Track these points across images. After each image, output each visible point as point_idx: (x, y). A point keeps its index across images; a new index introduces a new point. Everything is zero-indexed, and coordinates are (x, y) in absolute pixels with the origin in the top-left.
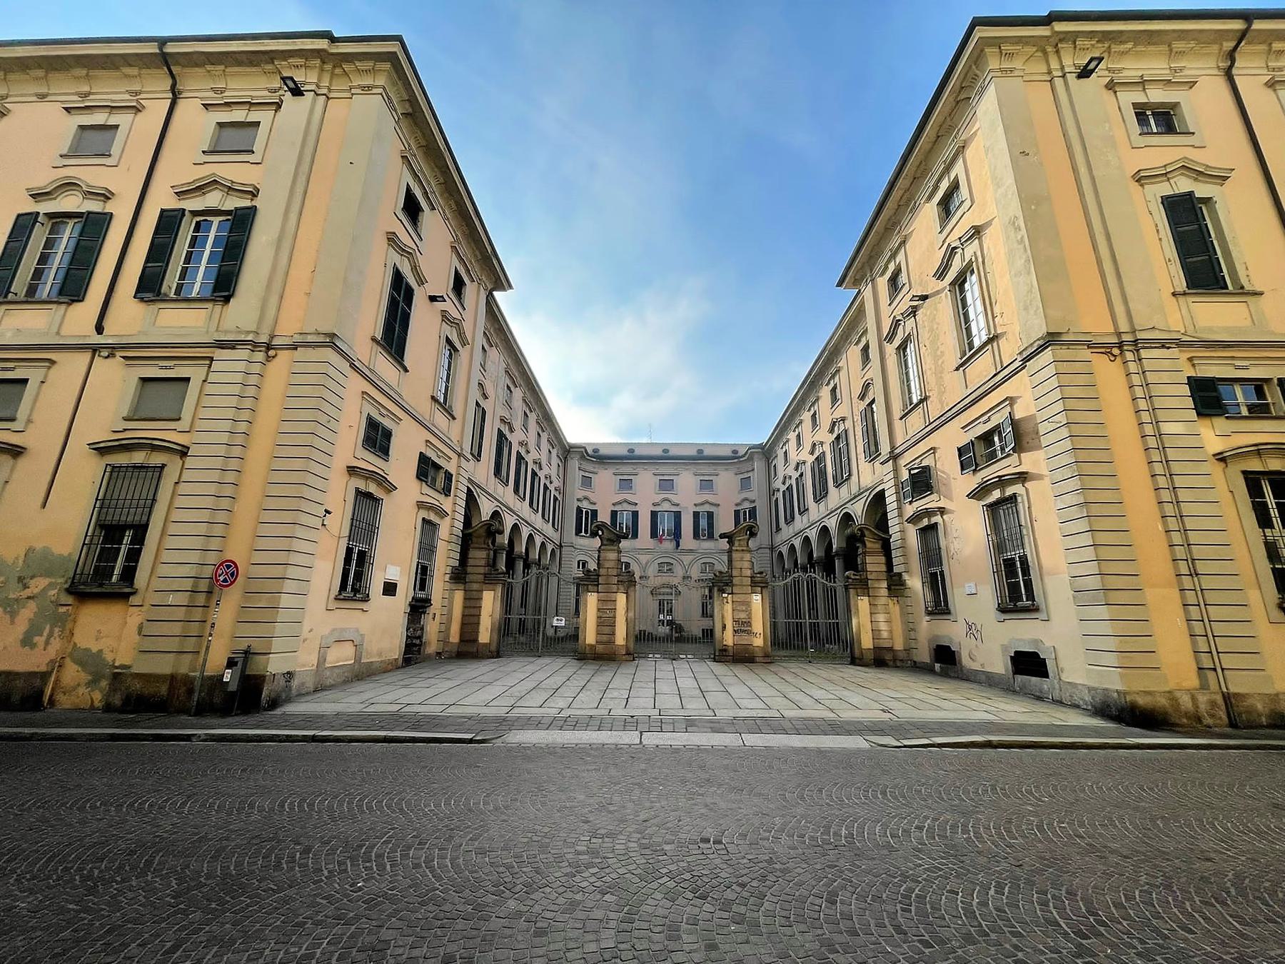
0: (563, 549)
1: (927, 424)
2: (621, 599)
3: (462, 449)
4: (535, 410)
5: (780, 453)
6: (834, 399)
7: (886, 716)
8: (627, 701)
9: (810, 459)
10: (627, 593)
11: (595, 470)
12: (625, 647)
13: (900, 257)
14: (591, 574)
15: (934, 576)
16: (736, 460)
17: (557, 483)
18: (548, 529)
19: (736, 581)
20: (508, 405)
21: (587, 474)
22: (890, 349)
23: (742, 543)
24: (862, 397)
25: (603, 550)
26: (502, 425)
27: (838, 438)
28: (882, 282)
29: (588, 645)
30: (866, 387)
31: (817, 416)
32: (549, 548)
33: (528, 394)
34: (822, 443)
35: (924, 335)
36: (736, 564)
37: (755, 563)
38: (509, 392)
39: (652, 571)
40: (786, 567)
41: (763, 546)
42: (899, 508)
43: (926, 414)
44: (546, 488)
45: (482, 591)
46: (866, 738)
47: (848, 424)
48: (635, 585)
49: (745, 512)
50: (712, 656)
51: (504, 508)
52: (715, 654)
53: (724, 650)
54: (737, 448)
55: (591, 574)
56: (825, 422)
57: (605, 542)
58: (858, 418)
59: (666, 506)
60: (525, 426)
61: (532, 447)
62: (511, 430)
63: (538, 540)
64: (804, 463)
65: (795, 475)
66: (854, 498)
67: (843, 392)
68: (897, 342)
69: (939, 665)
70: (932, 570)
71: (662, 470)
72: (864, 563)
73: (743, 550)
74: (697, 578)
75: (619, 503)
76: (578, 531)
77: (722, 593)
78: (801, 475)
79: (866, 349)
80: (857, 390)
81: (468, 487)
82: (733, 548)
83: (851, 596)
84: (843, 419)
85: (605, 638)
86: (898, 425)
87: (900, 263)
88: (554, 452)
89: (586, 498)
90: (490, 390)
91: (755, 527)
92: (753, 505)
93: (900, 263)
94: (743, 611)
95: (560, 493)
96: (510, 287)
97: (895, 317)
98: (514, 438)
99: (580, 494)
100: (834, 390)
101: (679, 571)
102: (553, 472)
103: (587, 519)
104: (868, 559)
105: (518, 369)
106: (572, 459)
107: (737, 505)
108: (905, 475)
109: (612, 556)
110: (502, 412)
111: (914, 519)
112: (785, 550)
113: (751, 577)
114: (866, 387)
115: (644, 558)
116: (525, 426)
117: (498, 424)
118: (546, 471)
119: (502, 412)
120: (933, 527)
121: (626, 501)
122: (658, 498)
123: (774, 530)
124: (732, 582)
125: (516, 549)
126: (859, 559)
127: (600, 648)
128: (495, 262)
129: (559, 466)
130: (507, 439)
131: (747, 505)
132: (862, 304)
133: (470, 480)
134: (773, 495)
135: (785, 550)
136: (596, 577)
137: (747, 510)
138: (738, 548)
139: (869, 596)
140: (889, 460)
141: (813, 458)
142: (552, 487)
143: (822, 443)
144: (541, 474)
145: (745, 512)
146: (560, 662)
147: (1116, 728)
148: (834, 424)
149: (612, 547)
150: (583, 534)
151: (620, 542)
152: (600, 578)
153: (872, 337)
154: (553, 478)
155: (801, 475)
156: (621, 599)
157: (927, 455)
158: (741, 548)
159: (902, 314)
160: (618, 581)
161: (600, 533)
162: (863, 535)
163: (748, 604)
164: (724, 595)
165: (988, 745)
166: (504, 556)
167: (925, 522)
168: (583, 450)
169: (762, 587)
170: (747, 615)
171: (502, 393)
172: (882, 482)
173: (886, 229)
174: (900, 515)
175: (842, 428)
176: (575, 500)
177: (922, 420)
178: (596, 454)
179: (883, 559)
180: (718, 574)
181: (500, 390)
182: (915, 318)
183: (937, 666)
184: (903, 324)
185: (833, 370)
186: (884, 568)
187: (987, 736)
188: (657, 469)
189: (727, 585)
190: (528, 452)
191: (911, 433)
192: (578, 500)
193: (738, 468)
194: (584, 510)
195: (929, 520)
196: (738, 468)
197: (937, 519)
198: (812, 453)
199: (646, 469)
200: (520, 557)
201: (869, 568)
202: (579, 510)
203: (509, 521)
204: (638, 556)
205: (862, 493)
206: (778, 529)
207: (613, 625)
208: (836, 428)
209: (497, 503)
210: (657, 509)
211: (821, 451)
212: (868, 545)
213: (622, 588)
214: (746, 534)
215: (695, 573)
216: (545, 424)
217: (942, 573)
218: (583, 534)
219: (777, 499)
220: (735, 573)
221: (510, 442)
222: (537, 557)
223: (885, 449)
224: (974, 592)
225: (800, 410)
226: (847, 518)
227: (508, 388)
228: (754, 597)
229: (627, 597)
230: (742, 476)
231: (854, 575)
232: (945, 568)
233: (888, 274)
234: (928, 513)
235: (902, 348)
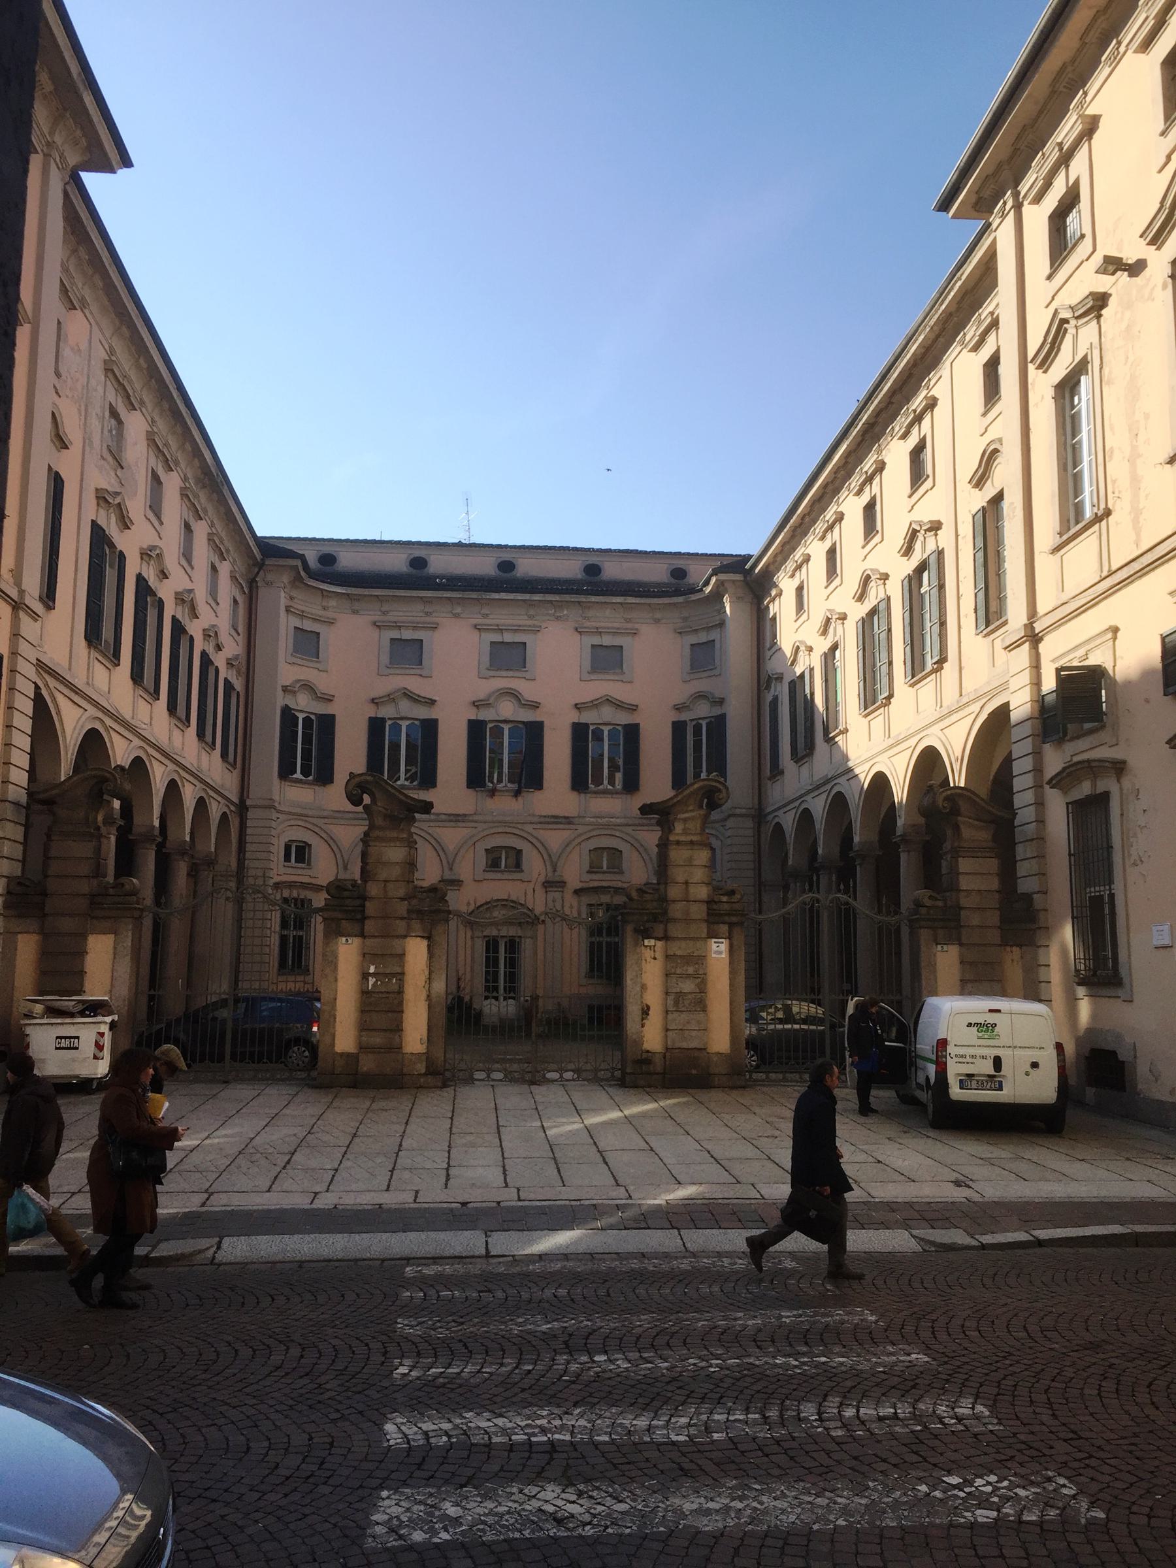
0: (250, 814)
1: (1105, 573)
2: (416, 951)
3: (22, 592)
4: (177, 463)
5: (786, 584)
6: (918, 473)
7: (960, 1194)
8: (448, 1175)
9: (858, 611)
10: (429, 938)
11: (330, 614)
12: (424, 1058)
13: (1078, 165)
14: (346, 894)
15: (1097, 902)
16: (681, 599)
17: (233, 647)
18: (213, 766)
19: (676, 910)
20: (116, 457)
21: (308, 625)
22: (1043, 385)
23: (690, 825)
24: (980, 480)
25: (378, 839)
26: (102, 512)
27: (922, 568)
28: (1037, 218)
29: (342, 1054)
30: (990, 458)
31: (878, 507)
32: (215, 810)
33: (162, 426)
34: (885, 577)
35: (1116, 367)
36: (679, 875)
37: (718, 852)
38: (113, 422)
39: (469, 867)
40: (790, 862)
41: (738, 811)
42: (1037, 754)
43: (1104, 551)
44: (206, 660)
45: (84, 937)
46: (915, 1232)
47: (945, 538)
48: (447, 921)
49: (697, 730)
50: (618, 1074)
51: (109, 722)
52: (623, 1070)
53: (645, 1060)
54: (680, 563)
55: (346, 894)
56: (894, 524)
57: (379, 821)
58: (966, 529)
59: (507, 710)
60: (155, 507)
61: (172, 560)
62: (125, 523)
63: (189, 795)
64: (843, 617)
65: (823, 645)
66: (950, 713)
67: (939, 459)
68: (1060, 368)
69: (1094, 1090)
70: (1093, 891)
71: (501, 617)
72: (955, 872)
73: (692, 842)
74: (579, 885)
75: (595, 705)
76: (286, 771)
77: (644, 938)
78: (835, 647)
79: (992, 367)
80: (969, 464)
81: (37, 687)
82: (672, 838)
83: (923, 942)
84: (935, 527)
85: (377, 1040)
86: (1045, 564)
87: (1077, 182)
88: (225, 569)
89: (308, 687)
90: (72, 429)
91: (719, 791)
92: (717, 711)
93: (1077, 182)
94: (689, 976)
95: (238, 673)
96: (127, 162)
97: (1056, 312)
98: (129, 543)
99: (288, 673)
100: (917, 454)
101: (535, 866)
102: (223, 623)
103: (307, 739)
104: (965, 865)
105: (137, 361)
106: (268, 584)
107: (678, 708)
108: (1049, 684)
109: (395, 854)
110: (100, 477)
111: (1061, 781)
112: (788, 821)
113: (708, 902)
114: (990, 458)
115: (555, 838)
116: (155, 507)
117: (91, 511)
118: (206, 617)
119: (100, 477)
120: (1101, 801)
121: (408, 695)
122: (484, 688)
123: (767, 772)
124: (665, 913)
125: (138, 819)
126: (944, 863)
127: (367, 1064)
128: (88, 99)
129: (235, 601)
130: (112, 546)
131: (703, 710)
132: (991, 255)
133: (40, 665)
134: (768, 687)
135: (788, 821)
136: (358, 902)
137: (704, 723)
138: (682, 838)
139: (961, 944)
140: (1024, 643)
141: (863, 609)
142: (219, 660)
143: (885, 577)
144: (195, 629)
145: (697, 730)
146: (275, 1095)
147: (644, 1199)
148: (913, 535)
149: (394, 834)
150: (298, 775)
151: (414, 820)
152: (368, 904)
153: (1006, 340)
154: (224, 638)
155: (835, 647)
156: (416, 951)
157: (1098, 641)
158: (689, 838)
159: (1072, 308)
160: (409, 911)
161: (367, 799)
162: (955, 811)
163: (700, 960)
164: (646, 942)
165: (1136, 1240)
166: (113, 839)
167: (1085, 789)
168: (299, 563)
169: (731, 925)
170: (698, 985)
171: (98, 427)
172: (1004, 687)
173: (1053, 92)
174: (1038, 770)
175: (931, 546)
176: (279, 689)
177: (1096, 565)
178: (328, 569)
179: (992, 864)
180: (634, 894)
181: (95, 424)
182: (1098, 323)
183: (1090, 1093)
184: (1074, 331)
185: (918, 403)
186: (994, 884)
187: (1131, 1226)
188: (486, 616)
189: (655, 918)
190: (163, 575)
191: (1071, 589)
192: (285, 689)
193: (685, 619)
194: (301, 716)
195: (1094, 785)
196: (685, 619)
197: (1106, 783)
198: (861, 597)
199: (457, 616)
200: (148, 838)
201: (965, 883)
202: (288, 715)
203: (159, 775)
204: (535, 833)
205: (967, 704)
206: (777, 771)
207: (397, 1009)
208: (918, 546)
209: (92, 711)
210: (485, 715)
211: (882, 595)
212: (966, 832)
213: (416, 924)
214: (701, 807)
215: (574, 872)
216: (203, 499)
217: (1112, 896)
218: (298, 775)
219: (776, 699)
220: (674, 892)
221: (122, 554)
222: (156, 823)
223: (1016, 613)
224: (1167, 942)
225: (837, 491)
226: (929, 761)
227: (114, 414)
228: (714, 946)
229: (429, 946)
230: (694, 639)
231: (930, 897)
232: (1118, 888)
233: (1051, 201)
234: (1092, 768)
235: (1067, 388)
